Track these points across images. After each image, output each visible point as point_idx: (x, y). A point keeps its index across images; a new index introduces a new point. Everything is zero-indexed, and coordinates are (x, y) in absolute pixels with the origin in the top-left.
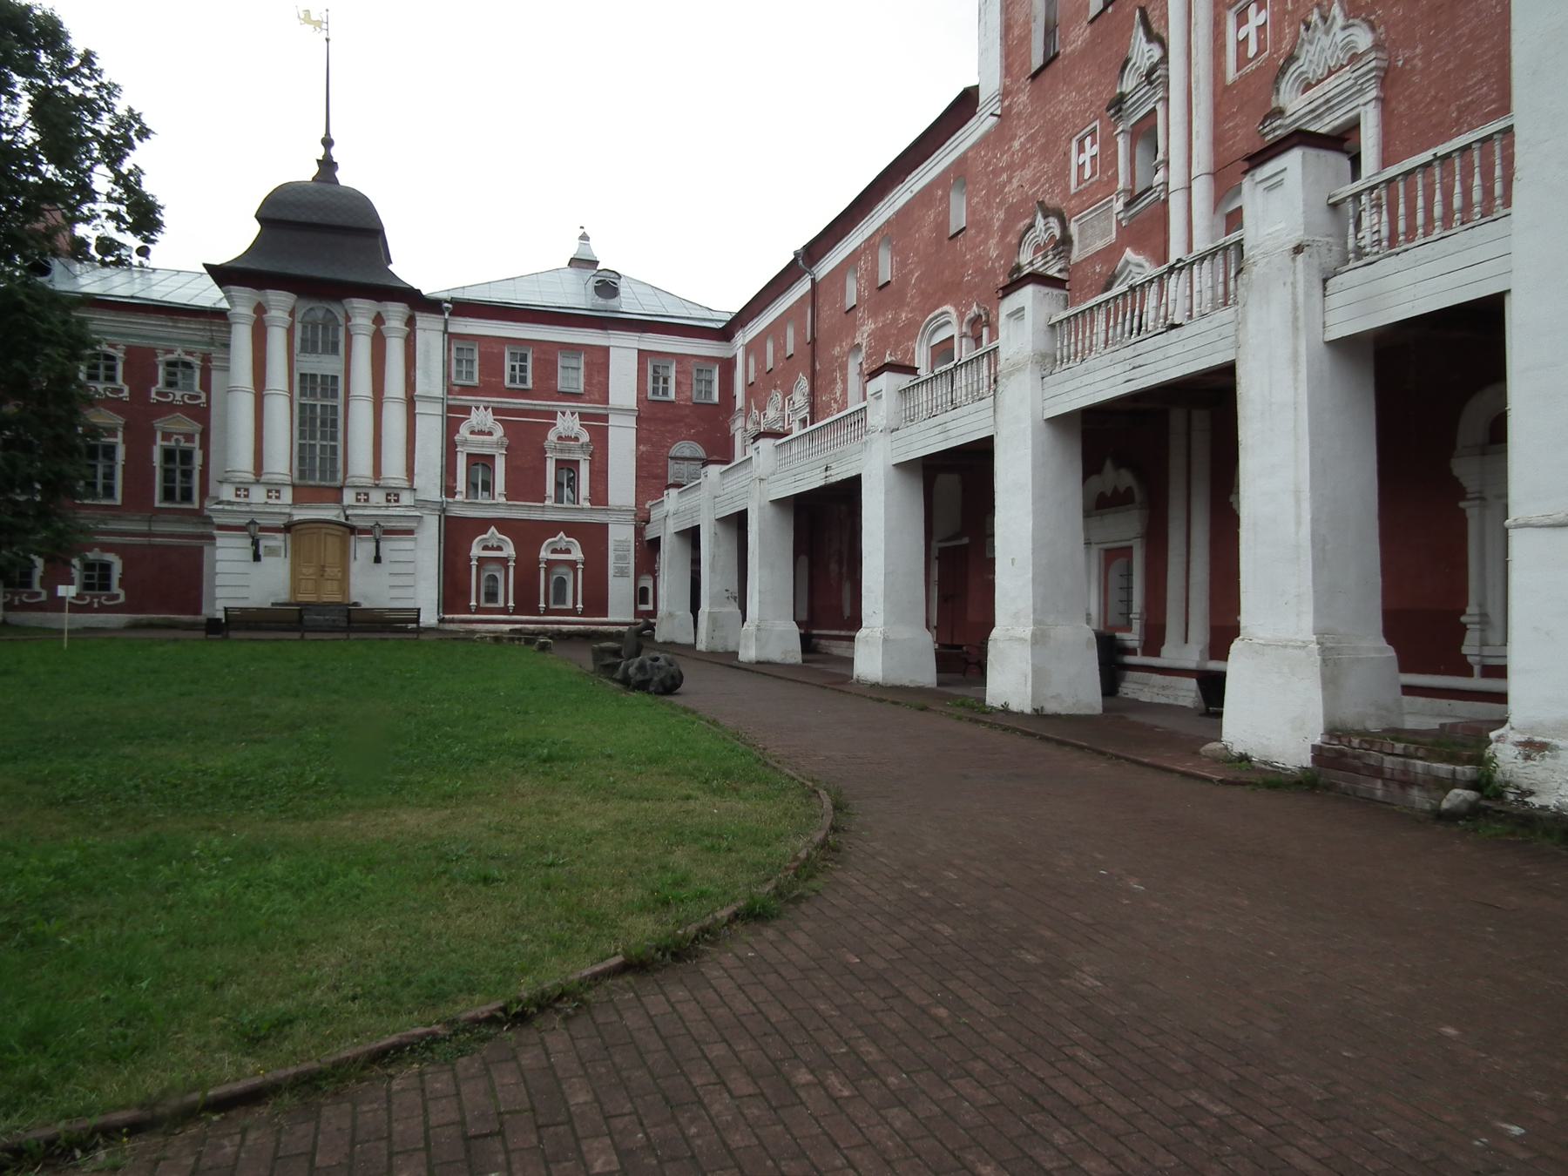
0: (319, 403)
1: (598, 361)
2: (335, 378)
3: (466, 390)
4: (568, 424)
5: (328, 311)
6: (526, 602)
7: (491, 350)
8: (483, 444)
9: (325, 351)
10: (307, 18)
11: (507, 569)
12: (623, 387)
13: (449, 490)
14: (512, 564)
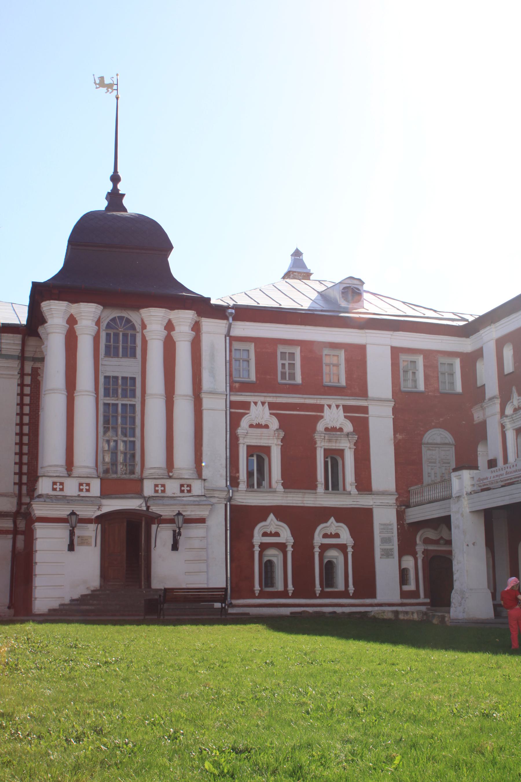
0: (120, 403)
2: (133, 379)
3: (246, 387)
6: (303, 587)
7: (266, 348)
9: (125, 355)
10: (101, 83)
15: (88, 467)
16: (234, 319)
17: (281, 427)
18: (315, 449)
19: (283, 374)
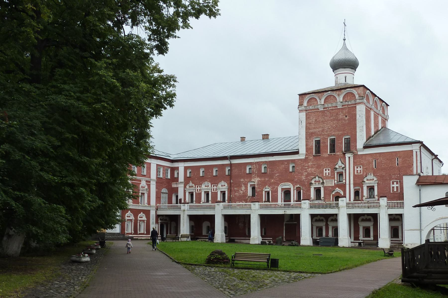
4: (143, 183)
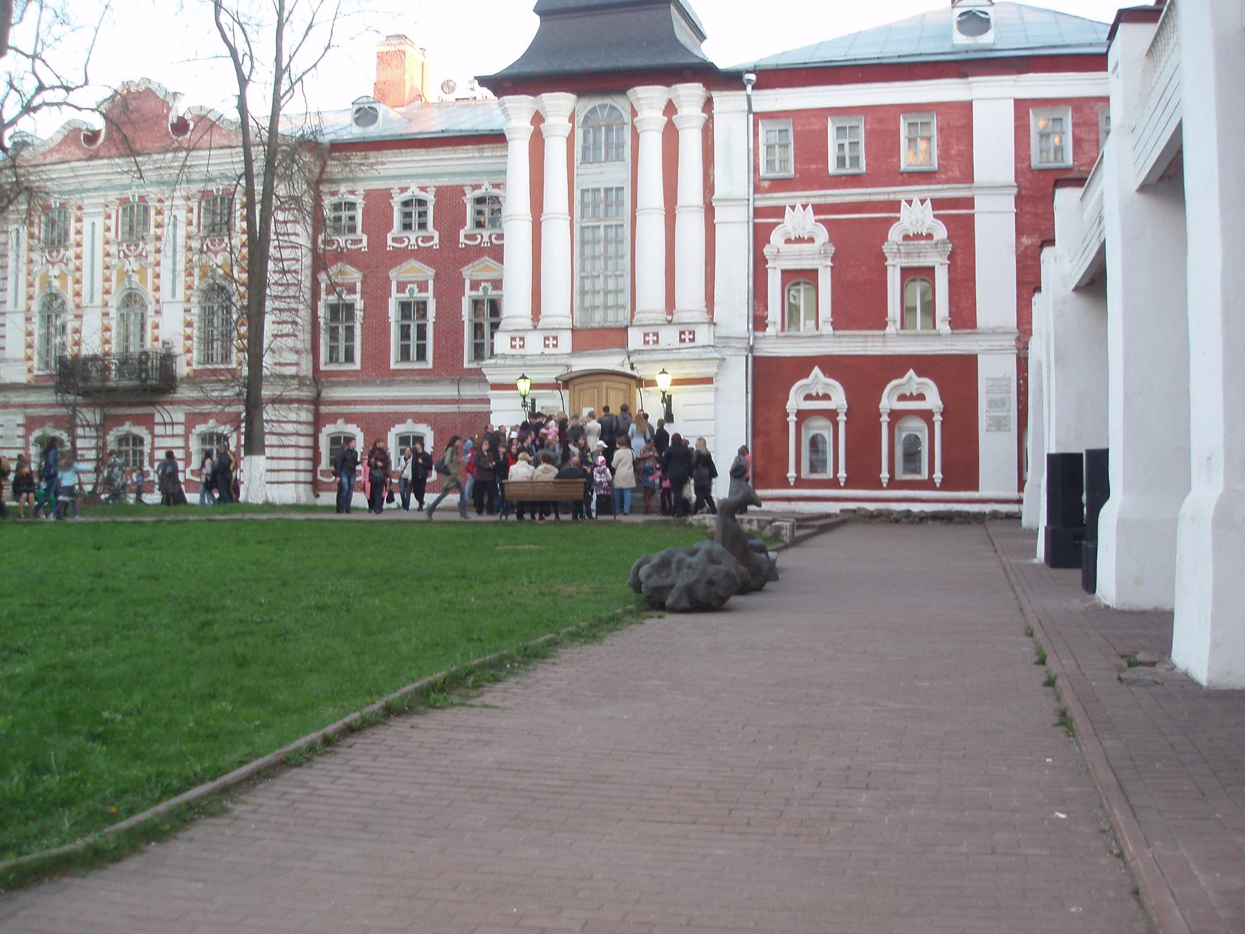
1: (957, 124)
3: (779, 184)
4: (916, 214)
5: (612, 108)
6: (863, 471)
8: (800, 256)
11: (836, 425)
12: (993, 156)
13: (759, 323)
14: (938, 418)
15: (655, 312)
16: (754, 88)
17: (832, 239)
18: (884, 270)
19: (841, 161)
